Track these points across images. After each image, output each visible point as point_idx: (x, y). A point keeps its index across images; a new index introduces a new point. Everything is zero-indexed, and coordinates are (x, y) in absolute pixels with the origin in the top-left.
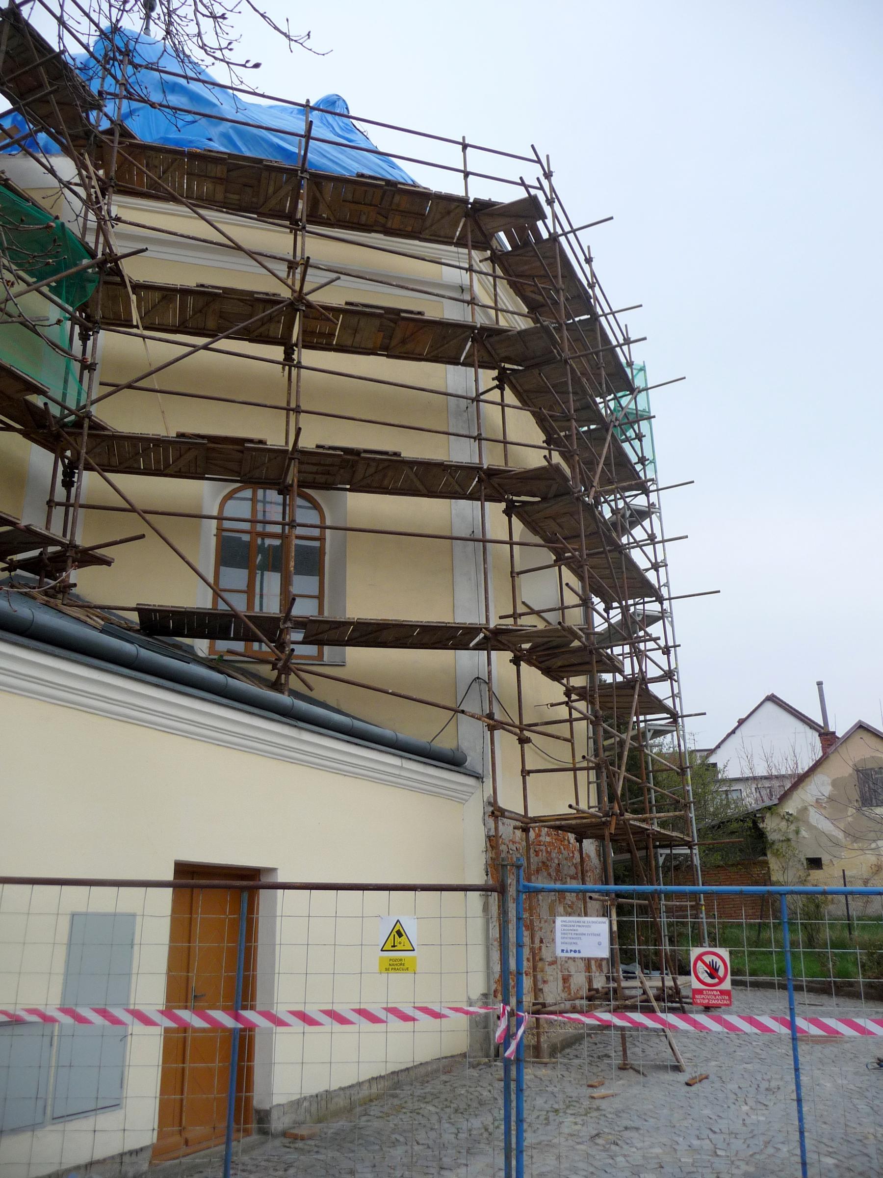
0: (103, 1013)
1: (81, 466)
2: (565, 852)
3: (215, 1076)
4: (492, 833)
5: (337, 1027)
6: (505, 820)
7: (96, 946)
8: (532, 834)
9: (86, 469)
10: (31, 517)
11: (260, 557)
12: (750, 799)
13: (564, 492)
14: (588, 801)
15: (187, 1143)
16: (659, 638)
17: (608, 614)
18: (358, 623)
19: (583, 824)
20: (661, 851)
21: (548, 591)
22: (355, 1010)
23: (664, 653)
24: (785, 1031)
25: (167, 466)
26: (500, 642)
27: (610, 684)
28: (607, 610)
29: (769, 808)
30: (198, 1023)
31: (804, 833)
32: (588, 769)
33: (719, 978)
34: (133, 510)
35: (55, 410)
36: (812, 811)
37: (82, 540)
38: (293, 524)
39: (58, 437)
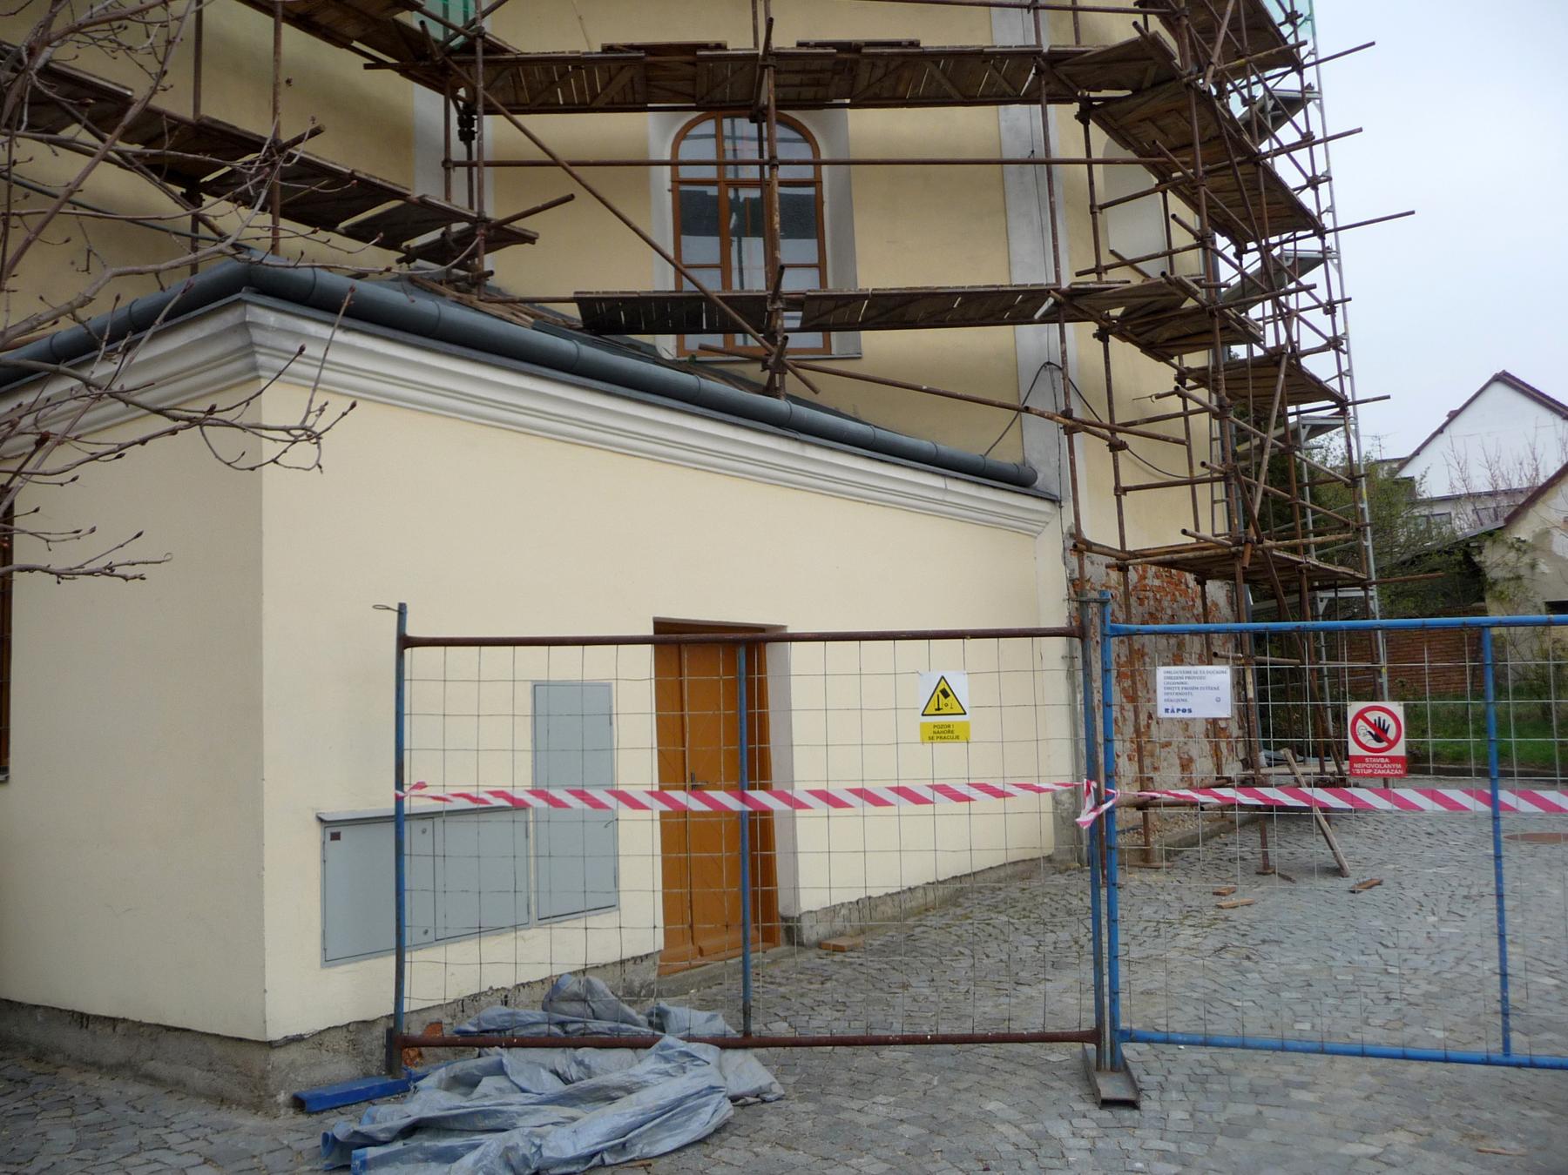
0: (581, 795)
1: (480, 108)
2: (1182, 600)
3: (730, 874)
4: (1076, 575)
5: (870, 809)
6: (1095, 556)
7: (566, 719)
8: (1133, 576)
9: (487, 112)
10: (425, 186)
11: (734, 216)
12: (1463, 524)
13: (1169, 76)
14: (1215, 524)
15: (701, 952)
16: (1314, 286)
17: (1241, 260)
18: (874, 295)
19: (1203, 558)
20: (1321, 594)
21: (1149, 230)
22: (892, 789)
23: (1326, 312)
24: (1483, 808)
25: (595, 96)
26: (1077, 308)
27: (1244, 361)
28: (1239, 255)
29: (1490, 534)
30: (696, 805)
31: (1543, 567)
32: (1212, 481)
33: (1388, 740)
34: (555, 163)
35: (436, 31)
36: (1556, 533)
37: (493, 212)
38: (774, 163)
39: (444, 69)
